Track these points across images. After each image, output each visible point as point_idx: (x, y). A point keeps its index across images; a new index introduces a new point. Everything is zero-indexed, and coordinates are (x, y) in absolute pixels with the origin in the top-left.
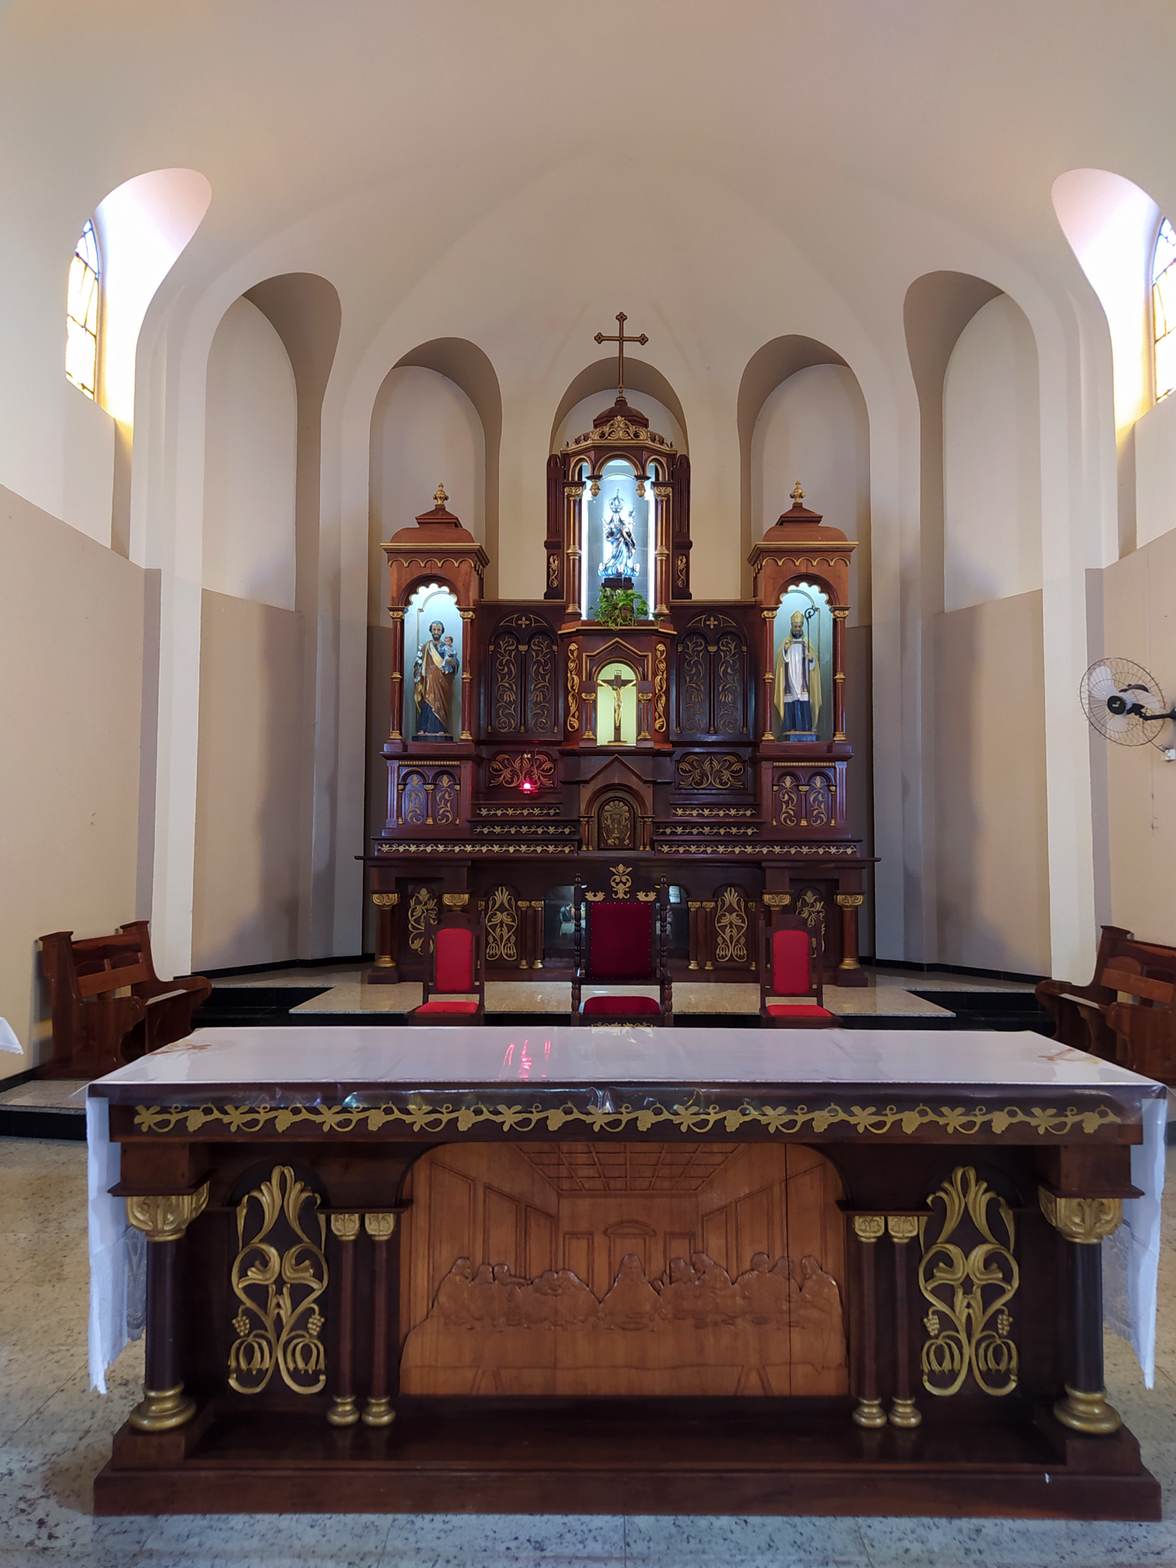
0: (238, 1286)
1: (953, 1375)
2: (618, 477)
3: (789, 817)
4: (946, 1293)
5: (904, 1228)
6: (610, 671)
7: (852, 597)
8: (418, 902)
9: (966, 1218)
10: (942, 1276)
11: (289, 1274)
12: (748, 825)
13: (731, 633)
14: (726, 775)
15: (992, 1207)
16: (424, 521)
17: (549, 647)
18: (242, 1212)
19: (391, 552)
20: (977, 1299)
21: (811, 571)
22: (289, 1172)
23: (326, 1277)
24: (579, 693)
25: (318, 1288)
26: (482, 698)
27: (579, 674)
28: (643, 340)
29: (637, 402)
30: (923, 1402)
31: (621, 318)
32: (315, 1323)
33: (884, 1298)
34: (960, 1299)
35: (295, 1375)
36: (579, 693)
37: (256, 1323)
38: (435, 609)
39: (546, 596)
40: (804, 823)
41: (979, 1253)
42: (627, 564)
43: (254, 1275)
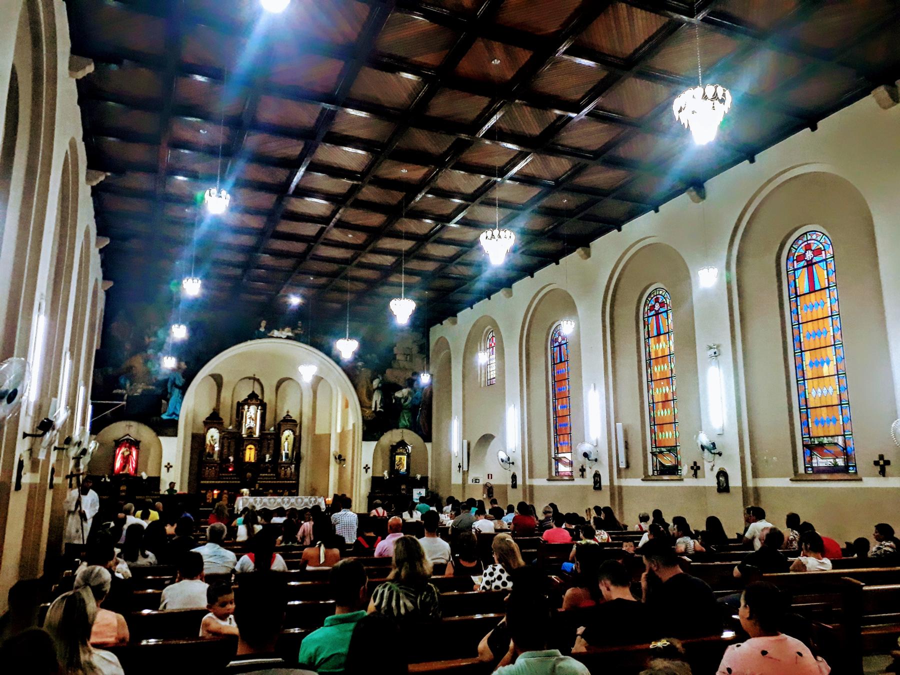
2: (253, 408)
6: (249, 446)
7: (297, 434)
22: (608, 582)
23: (64, 546)
26: (96, 337)
38: (213, 434)
42: (252, 424)
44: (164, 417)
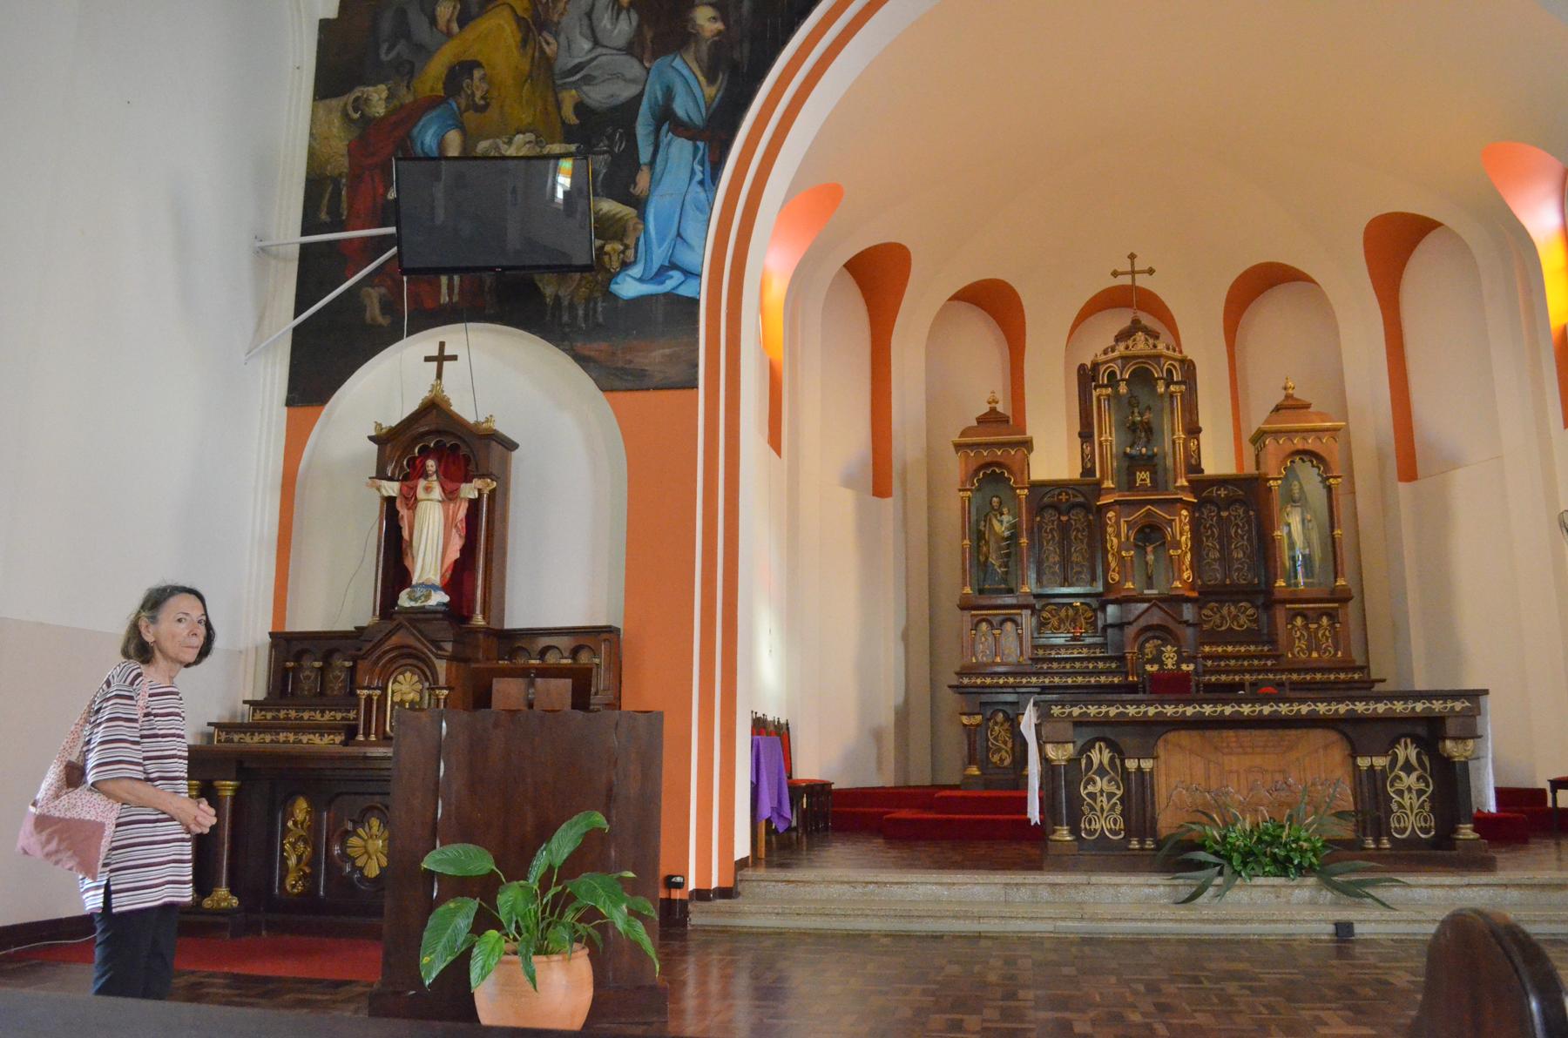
0: (1083, 793)
1: (1405, 829)
3: (1302, 650)
4: (1400, 793)
5: (1380, 762)
8: (996, 723)
9: (1407, 761)
10: (1398, 785)
11: (1105, 788)
12: (1268, 657)
13: (1236, 501)
14: (1243, 619)
15: (1419, 755)
16: (982, 420)
17: (1086, 516)
18: (1084, 762)
19: (958, 447)
20: (1414, 795)
21: (1307, 447)
24: (1119, 552)
25: (1119, 793)
27: (1118, 535)
28: (1151, 271)
29: (1147, 320)
30: (1392, 840)
31: (1132, 257)
32: (1119, 808)
33: (1372, 791)
34: (1406, 795)
35: (1110, 831)
36: (1119, 552)
37: (1092, 809)
39: (1082, 475)
40: (1315, 655)
41: (1414, 776)
43: (1090, 788)
44: (628, 287)
